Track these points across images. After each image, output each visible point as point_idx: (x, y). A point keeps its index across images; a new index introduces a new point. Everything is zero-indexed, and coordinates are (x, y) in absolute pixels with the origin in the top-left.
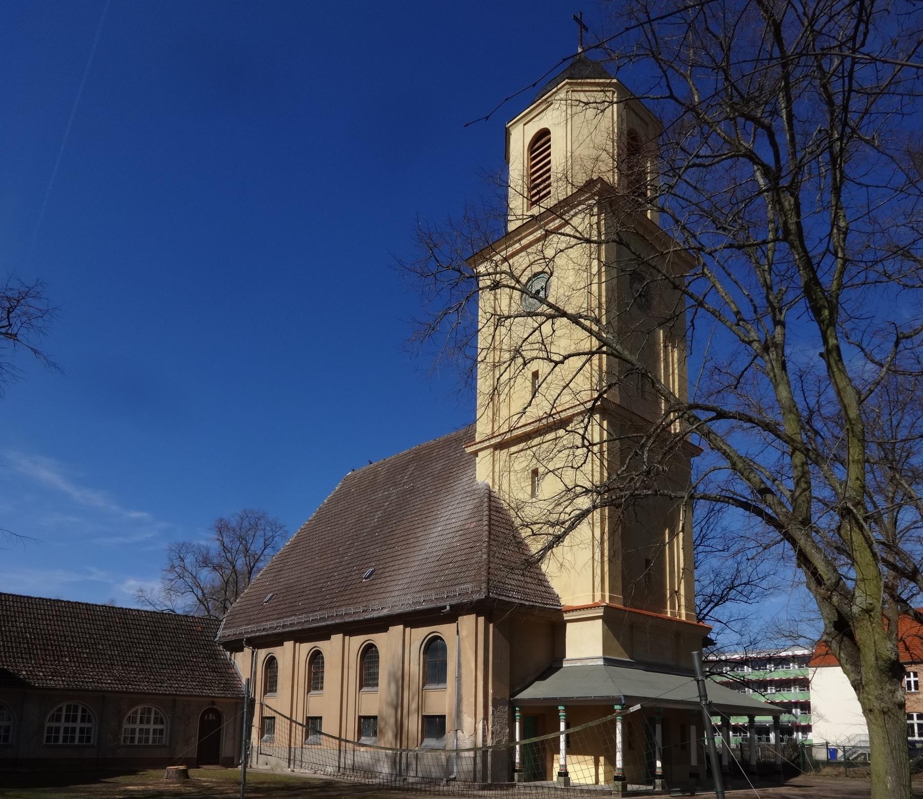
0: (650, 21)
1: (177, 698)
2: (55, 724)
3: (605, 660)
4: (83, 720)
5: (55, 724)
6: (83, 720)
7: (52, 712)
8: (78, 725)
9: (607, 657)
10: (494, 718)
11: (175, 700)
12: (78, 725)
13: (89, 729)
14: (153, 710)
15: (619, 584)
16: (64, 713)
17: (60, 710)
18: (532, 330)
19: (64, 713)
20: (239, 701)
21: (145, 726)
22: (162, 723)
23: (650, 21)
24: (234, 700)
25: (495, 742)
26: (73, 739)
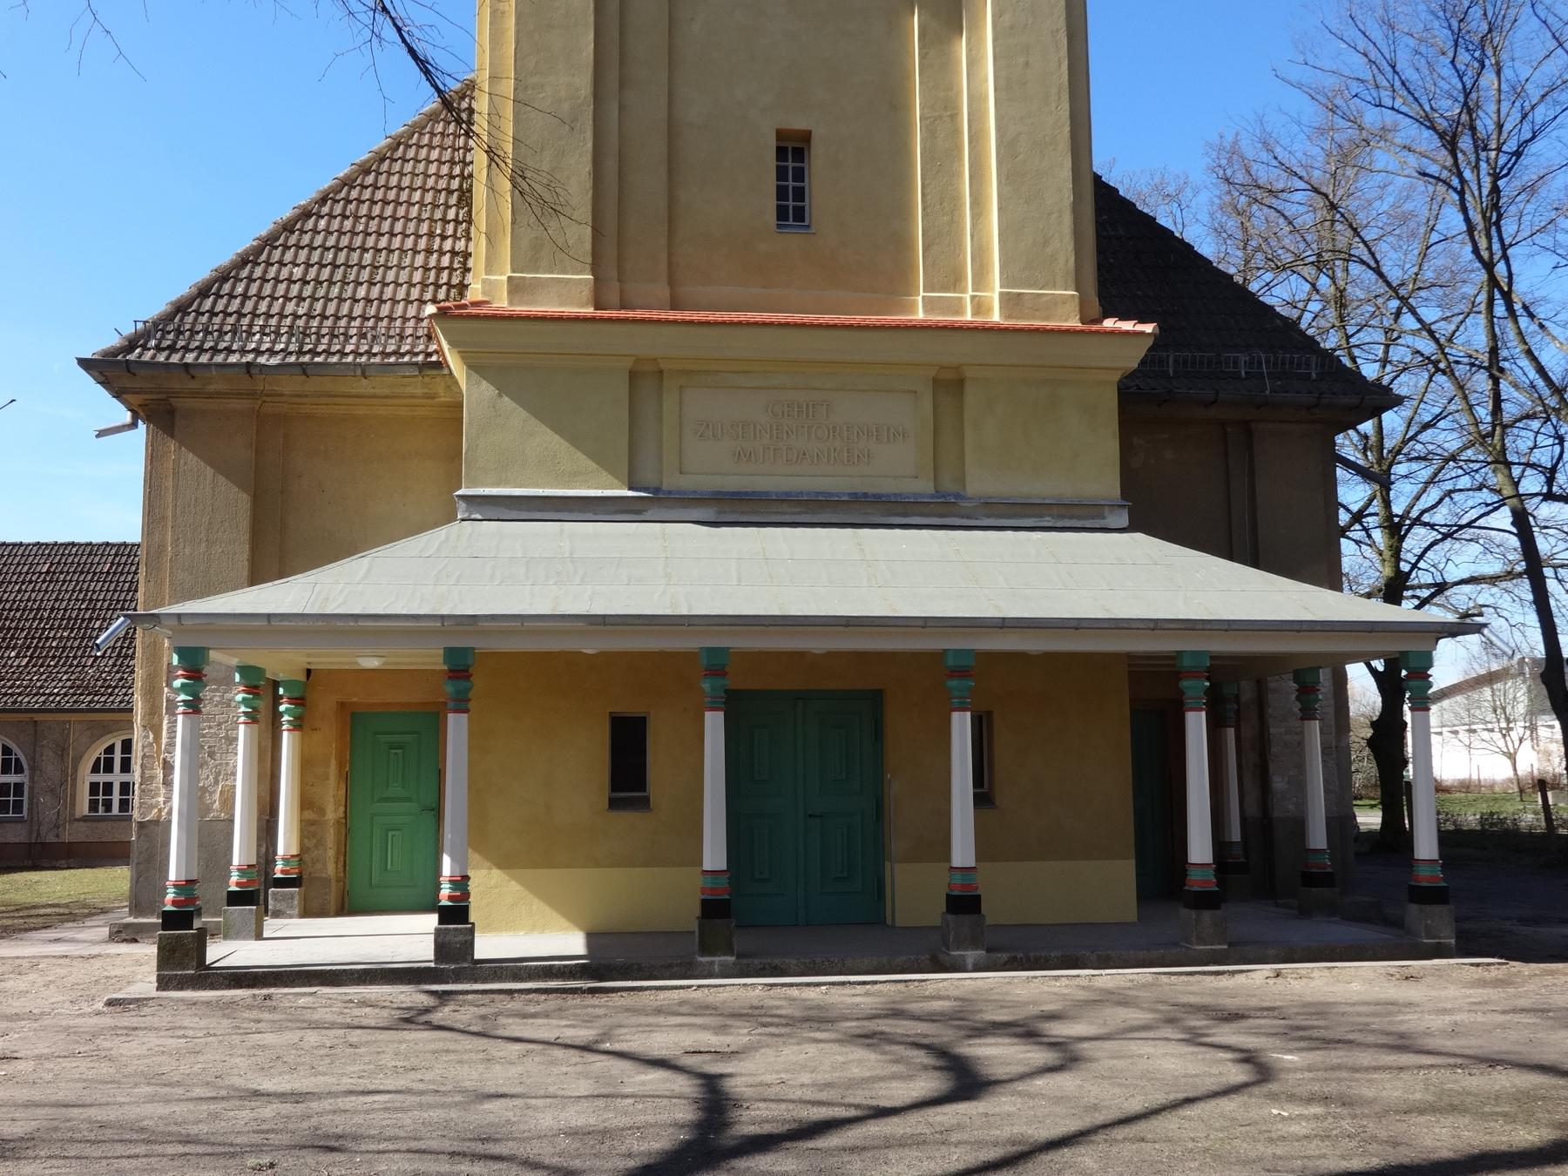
5: (102, 778)
7: (96, 755)
17: (110, 750)
26: (108, 805)
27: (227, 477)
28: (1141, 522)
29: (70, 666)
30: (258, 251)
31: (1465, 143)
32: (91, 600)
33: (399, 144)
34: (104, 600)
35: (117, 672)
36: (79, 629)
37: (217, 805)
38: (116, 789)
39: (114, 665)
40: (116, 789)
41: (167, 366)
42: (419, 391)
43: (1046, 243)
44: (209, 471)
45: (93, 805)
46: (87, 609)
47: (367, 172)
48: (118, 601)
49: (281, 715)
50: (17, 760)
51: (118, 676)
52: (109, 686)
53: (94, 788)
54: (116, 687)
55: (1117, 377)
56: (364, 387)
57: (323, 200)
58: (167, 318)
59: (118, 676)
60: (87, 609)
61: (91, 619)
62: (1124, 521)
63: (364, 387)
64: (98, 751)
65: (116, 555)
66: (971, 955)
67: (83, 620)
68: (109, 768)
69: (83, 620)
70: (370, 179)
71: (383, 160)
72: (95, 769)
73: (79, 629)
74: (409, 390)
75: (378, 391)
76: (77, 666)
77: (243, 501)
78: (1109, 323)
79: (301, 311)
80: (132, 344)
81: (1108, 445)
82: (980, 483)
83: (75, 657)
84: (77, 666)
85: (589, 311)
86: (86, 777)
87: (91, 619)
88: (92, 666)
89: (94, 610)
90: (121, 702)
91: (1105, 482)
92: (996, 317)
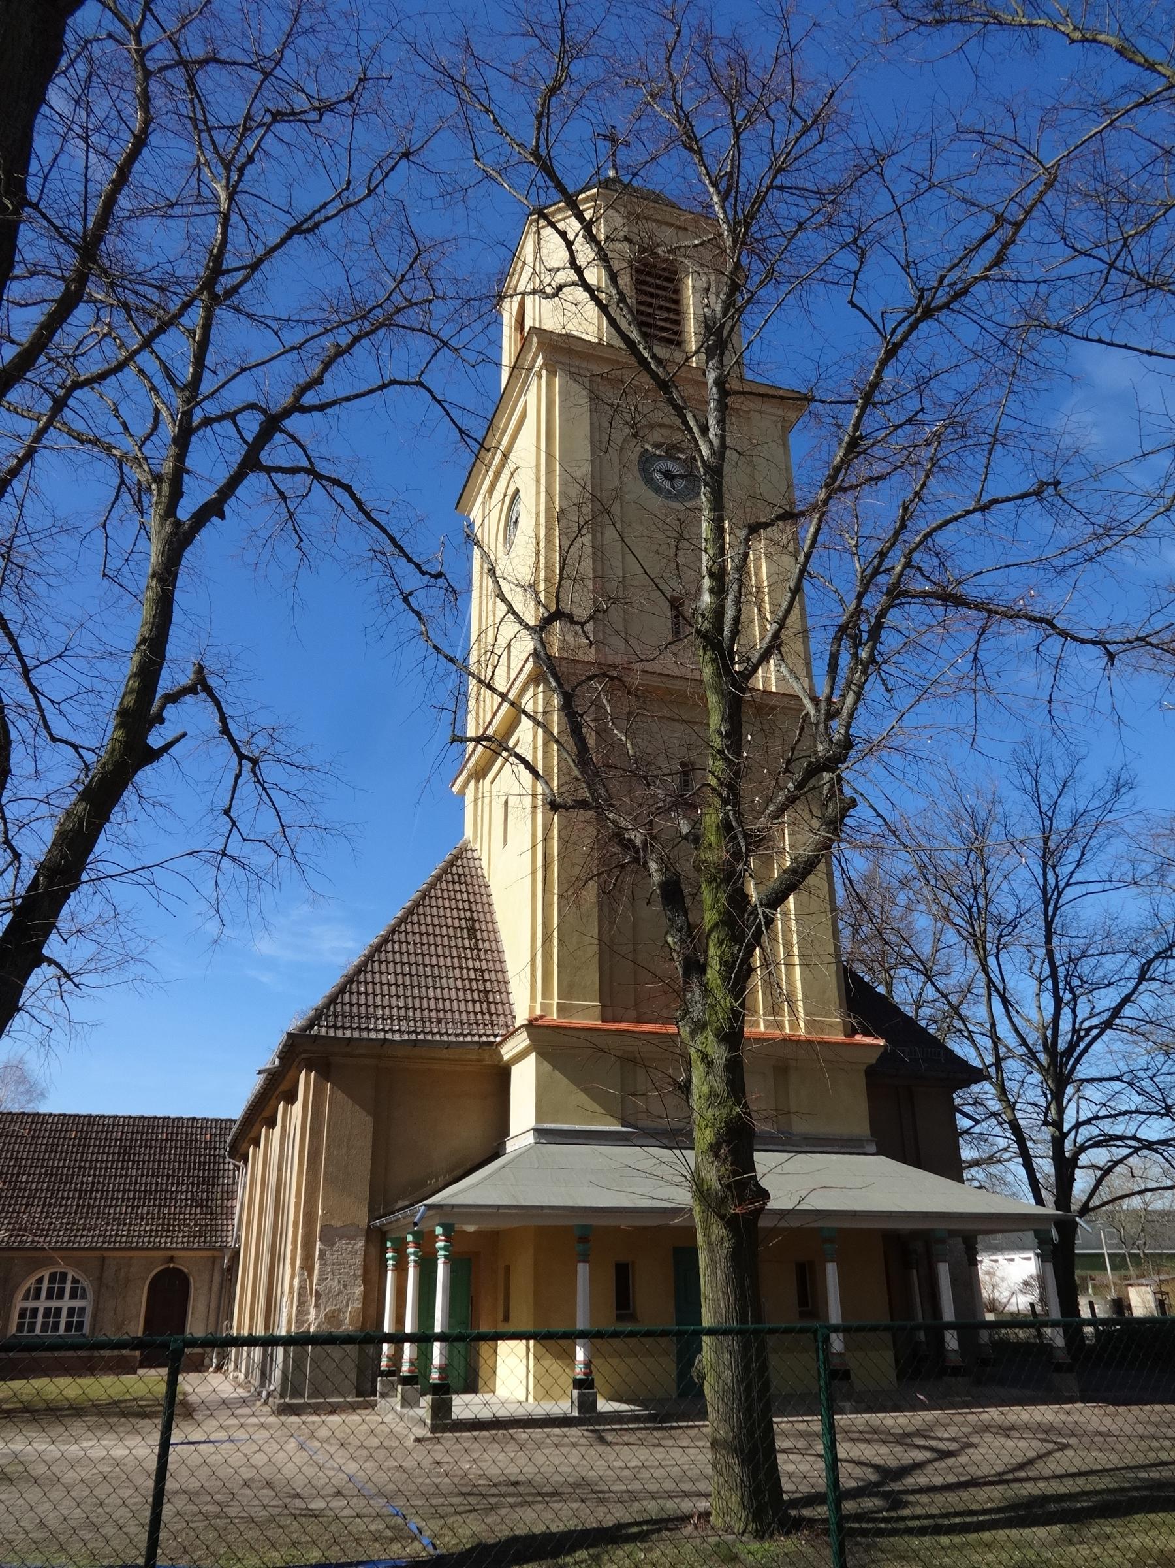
0: (1112, 265)
1: (106, 1254)
2: (30, 1304)
3: (539, 1132)
4: (73, 1296)
5: (30, 1304)
6: (73, 1296)
7: (28, 1286)
8: (66, 1304)
9: (541, 1126)
10: (324, 1265)
11: (104, 1259)
12: (66, 1304)
13: (82, 1309)
14: (70, 1277)
15: (592, 978)
16: (45, 1286)
17: (40, 1281)
18: (328, 411)
19: (45, 1286)
20: (216, 1253)
21: (54, 1304)
22: (84, 1297)
23: (1112, 265)
24: (209, 1253)
25: (322, 1314)
26: (56, 1326)
27: (362, 1107)
28: (883, 1150)
29: (8, 1212)
30: (365, 964)
31: (975, 910)
32: (17, 1159)
33: (425, 896)
34: (27, 1159)
35: (46, 1218)
36: (10, 1182)
37: (347, 1321)
38: (41, 1313)
39: (42, 1212)
40: (41, 1313)
41: (335, 1038)
42: (474, 1057)
43: (824, 992)
44: (350, 1102)
45: (20, 1326)
46: (14, 1166)
47: (412, 914)
48: (38, 1160)
49: (387, 1260)
50: (83, 1289)
51: (48, 1221)
52: (43, 1229)
53: (22, 1314)
54: (49, 1230)
55: (864, 1067)
56: (444, 1054)
57: (393, 932)
58: (327, 1006)
59: (48, 1221)
60: (14, 1166)
61: (18, 1174)
62: (873, 1149)
63: (444, 1054)
64: (30, 1282)
65: (32, 1123)
66: (847, 1405)
67: (13, 1175)
68: (37, 1297)
69: (13, 1175)
70: (415, 918)
71: (418, 906)
72: (26, 1298)
73: (10, 1182)
74: (469, 1057)
75: (452, 1057)
76: (13, 1212)
77: (370, 1119)
78: (859, 1038)
79: (401, 1005)
80: (313, 1022)
81: (861, 1106)
82: (800, 1126)
83: (10, 1205)
84: (13, 1212)
85: (598, 1024)
86: (19, 1304)
87: (18, 1174)
88: (24, 1213)
89: (20, 1167)
90: (57, 1242)
91: (861, 1127)
92: (802, 1032)
